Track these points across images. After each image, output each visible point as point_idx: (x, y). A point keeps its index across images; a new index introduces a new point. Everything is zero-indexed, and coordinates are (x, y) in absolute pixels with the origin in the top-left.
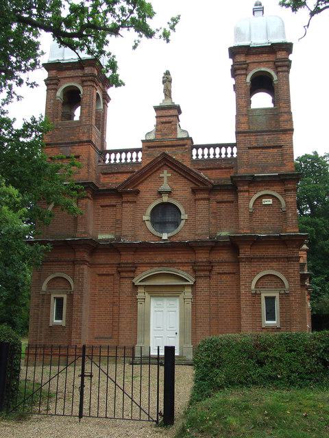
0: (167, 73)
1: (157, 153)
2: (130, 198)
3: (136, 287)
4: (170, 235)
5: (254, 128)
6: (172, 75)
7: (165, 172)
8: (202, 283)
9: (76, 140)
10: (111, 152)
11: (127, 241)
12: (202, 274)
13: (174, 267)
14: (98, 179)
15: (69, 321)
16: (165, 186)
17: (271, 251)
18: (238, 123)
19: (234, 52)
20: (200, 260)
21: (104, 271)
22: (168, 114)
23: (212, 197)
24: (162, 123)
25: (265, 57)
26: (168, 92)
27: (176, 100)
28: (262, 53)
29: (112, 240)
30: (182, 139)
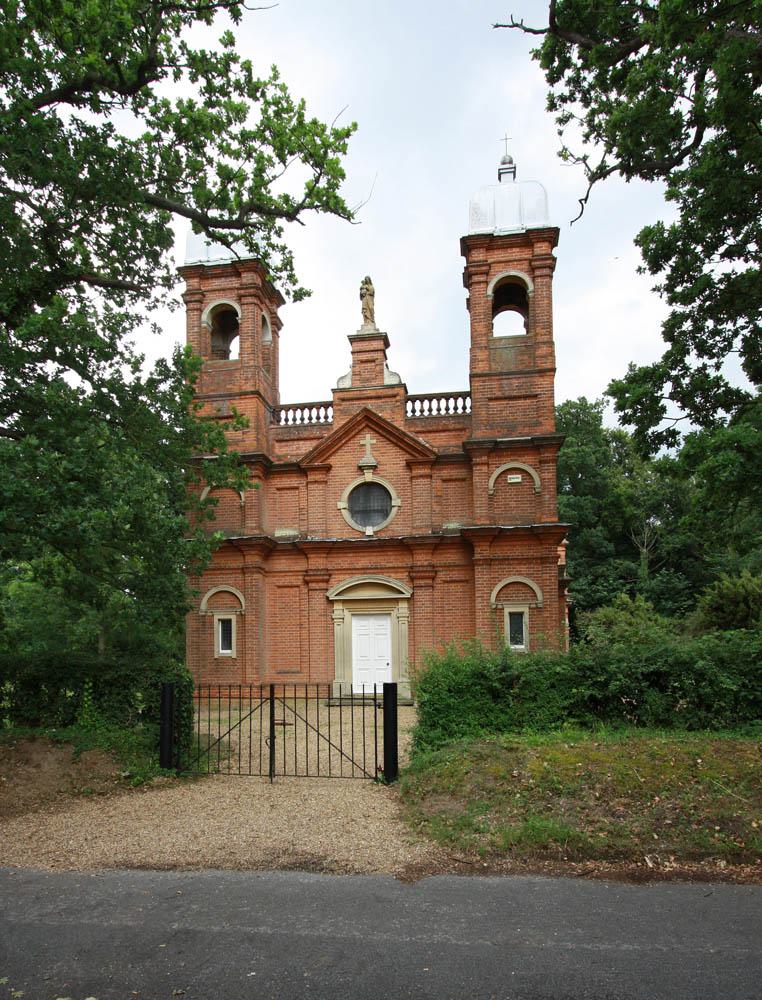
0: (368, 281)
1: (356, 408)
2: (318, 476)
3: (331, 602)
4: (376, 529)
5: (497, 368)
6: (376, 285)
7: (368, 436)
8: (423, 596)
9: (236, 390)
10: (287, 408)
11: (317, 539)
12: (422, 582)
13: (378, 573)
14: (271, 448)
15: (242, 652)
16: (368, 459)
17: (518, 550)
18: (473, 361)
19: (468, 245)
20: (419, 563)
21: (286, 581)
22: (370, 346)
23: (436, 474)
24: (362, 362)
25: (515, 253)
26: (368, 314)
27: (382, 324)
28: (511, 246)
29: (295, 537)
30: (392, 387)
